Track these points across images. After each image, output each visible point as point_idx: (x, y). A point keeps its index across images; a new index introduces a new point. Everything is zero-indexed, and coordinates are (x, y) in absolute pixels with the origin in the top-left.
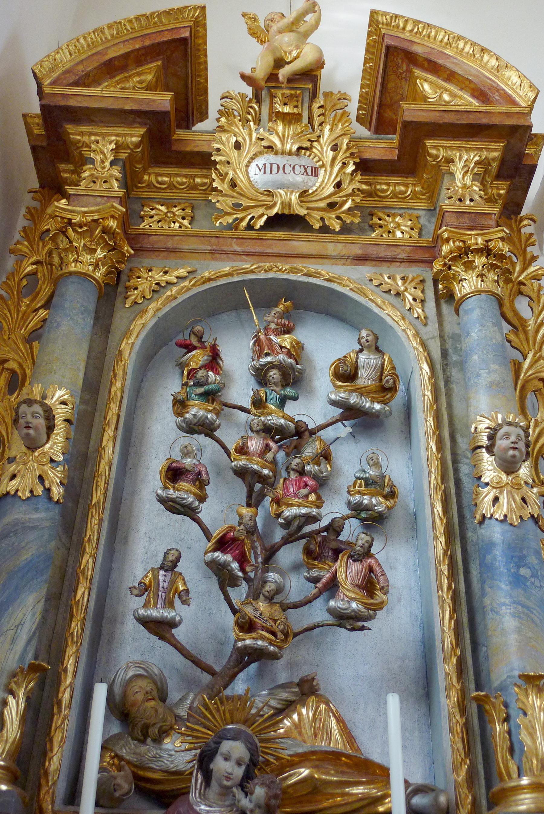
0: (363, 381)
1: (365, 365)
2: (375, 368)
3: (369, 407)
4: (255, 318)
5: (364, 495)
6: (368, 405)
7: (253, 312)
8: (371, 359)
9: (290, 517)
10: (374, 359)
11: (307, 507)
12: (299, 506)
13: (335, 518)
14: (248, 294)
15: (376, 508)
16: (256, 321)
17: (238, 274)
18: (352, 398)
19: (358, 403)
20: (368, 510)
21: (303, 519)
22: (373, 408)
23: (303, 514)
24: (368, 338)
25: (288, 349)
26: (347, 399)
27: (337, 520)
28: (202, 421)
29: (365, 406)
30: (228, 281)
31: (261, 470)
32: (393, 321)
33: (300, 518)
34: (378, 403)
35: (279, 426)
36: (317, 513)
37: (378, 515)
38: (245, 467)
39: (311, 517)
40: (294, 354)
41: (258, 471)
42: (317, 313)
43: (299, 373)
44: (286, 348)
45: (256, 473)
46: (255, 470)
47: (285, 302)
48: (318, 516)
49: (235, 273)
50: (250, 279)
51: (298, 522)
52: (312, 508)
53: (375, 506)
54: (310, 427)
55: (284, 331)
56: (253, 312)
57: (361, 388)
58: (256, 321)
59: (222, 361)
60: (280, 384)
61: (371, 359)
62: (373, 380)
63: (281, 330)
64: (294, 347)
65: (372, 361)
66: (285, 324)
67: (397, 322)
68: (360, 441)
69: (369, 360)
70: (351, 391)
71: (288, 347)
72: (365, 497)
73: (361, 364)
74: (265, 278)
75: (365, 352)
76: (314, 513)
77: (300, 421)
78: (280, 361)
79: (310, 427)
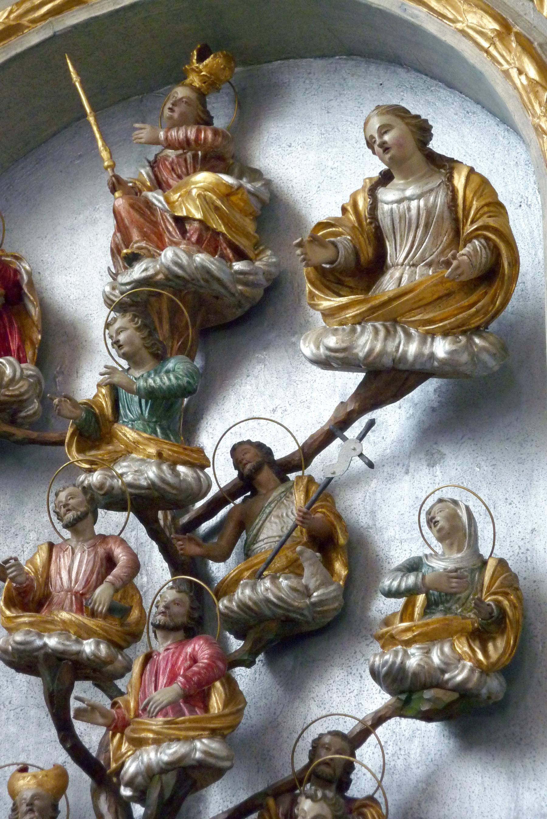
0: (397, 275)
1: (397, 225)
2: (427, 226)
3: (419, 355)
4: (100, 143)
5: (408, 643)
6: (413, 349)
7: (95, 128)
8: (410, 199)
9: (140, 779)
10: (419, 197)
11: (178, 740)
12: (157, 742)
13: (321, 736)
14: (78, 73)
15: (447, 676)
16: (105, 154)
17: (34, 21)
18: (362, 340)
19: (383, 353)
20: (426, 686)
21: (170, 779)
22: (432, 356)
23: (168, 764)
24: (386, 138)
25: (200, 221)
26: (344, 350)
27: (327, 739)
28: (375, 358)
29: (405, 353)
30: (13, 53)
31: (75, 648)
32: (477, 50)
33: (164, 777)
34: (445, 334)
35: (148, 488)
36: (205, 752)
37: (456, 696)
38: (24, 651)
39: (192, 767)
40: (223, 229)
41: (63, 652)
42: (323, 56)
43: (246, 284)
44: (195, 220)
45: (60, 659)
46: (55, 651)
47: (201, 59)
48: (211, 760)
49: (25, 21)
50: (75, 27)
51: (159, 788)
52: (194, 738)
53: (443, 672)
54: (279, 454)
55: (204, 157)
56: (95, 128)
57: (391, 300)
58: (105, 154)
59: (109, 269)
60: (145, 353)
61: (410, 199)
62: (429, 265)
63: (195, 156)
64: (217, 209)
65: (414, 204)
66: (187, 140)
67: (487, 51)
68: (443, 456)
69: (405, 204)
70: (361, 320)
71: (198, 215)
72: (412, 650)
73: (385, 223)
74: (117, 11)
75: (397, 181)
76: (198, 755)
77: (241, 444)
78: (168, 269)
79: (279, 454)
